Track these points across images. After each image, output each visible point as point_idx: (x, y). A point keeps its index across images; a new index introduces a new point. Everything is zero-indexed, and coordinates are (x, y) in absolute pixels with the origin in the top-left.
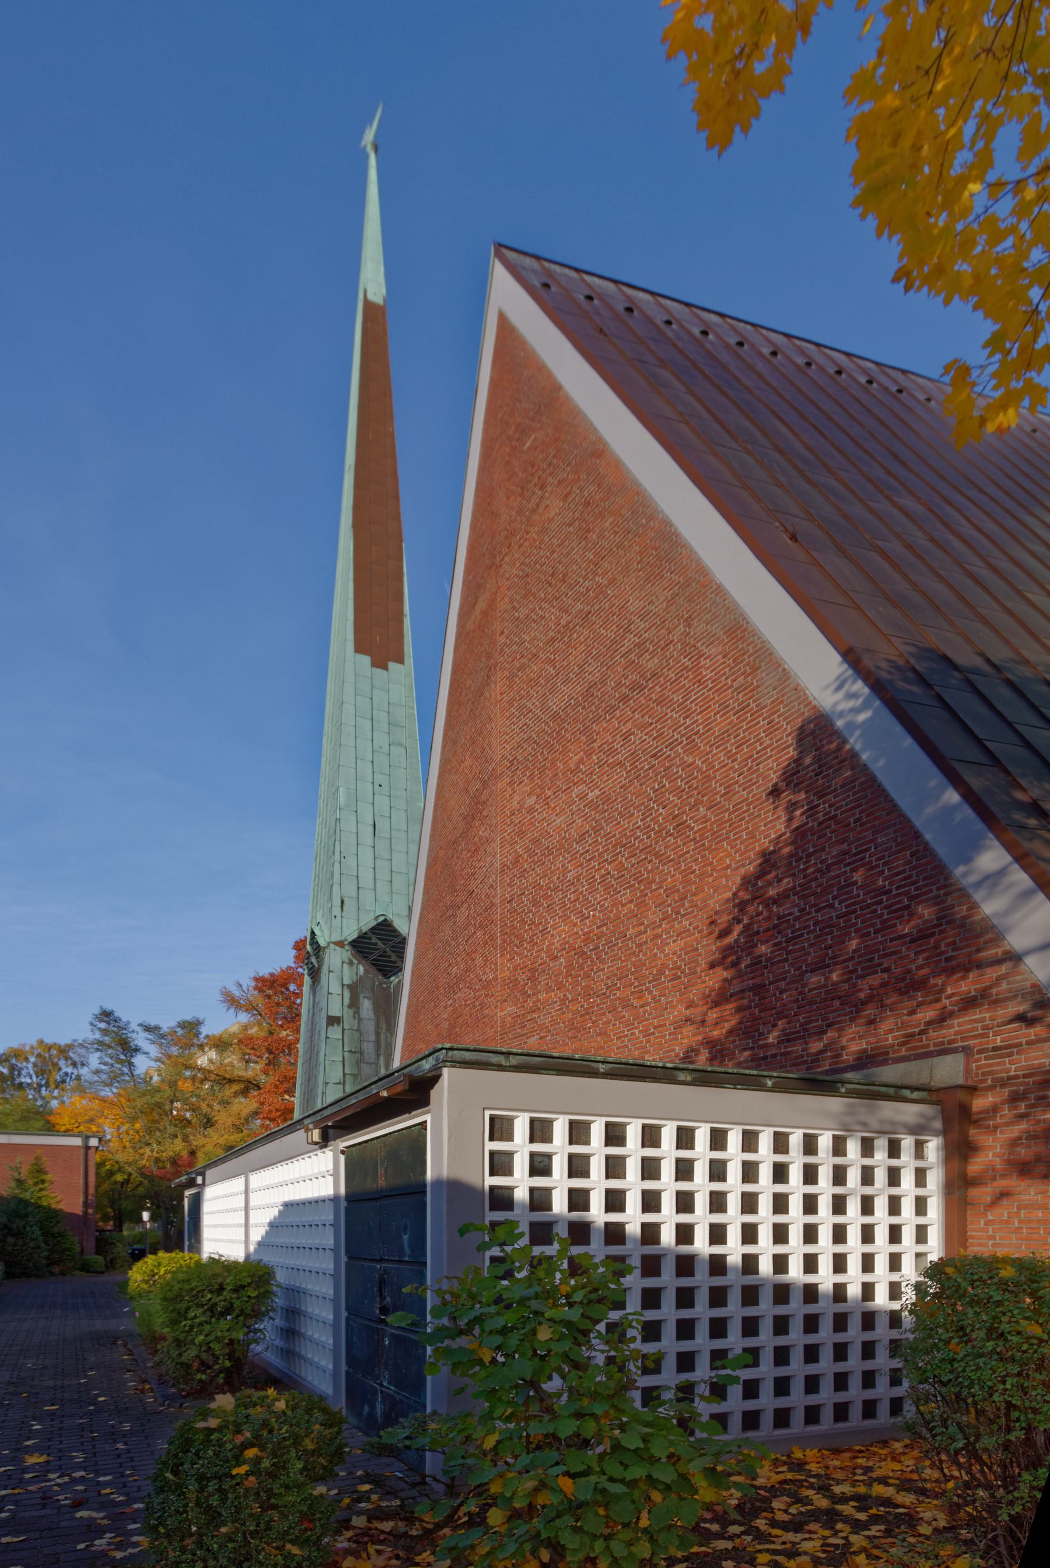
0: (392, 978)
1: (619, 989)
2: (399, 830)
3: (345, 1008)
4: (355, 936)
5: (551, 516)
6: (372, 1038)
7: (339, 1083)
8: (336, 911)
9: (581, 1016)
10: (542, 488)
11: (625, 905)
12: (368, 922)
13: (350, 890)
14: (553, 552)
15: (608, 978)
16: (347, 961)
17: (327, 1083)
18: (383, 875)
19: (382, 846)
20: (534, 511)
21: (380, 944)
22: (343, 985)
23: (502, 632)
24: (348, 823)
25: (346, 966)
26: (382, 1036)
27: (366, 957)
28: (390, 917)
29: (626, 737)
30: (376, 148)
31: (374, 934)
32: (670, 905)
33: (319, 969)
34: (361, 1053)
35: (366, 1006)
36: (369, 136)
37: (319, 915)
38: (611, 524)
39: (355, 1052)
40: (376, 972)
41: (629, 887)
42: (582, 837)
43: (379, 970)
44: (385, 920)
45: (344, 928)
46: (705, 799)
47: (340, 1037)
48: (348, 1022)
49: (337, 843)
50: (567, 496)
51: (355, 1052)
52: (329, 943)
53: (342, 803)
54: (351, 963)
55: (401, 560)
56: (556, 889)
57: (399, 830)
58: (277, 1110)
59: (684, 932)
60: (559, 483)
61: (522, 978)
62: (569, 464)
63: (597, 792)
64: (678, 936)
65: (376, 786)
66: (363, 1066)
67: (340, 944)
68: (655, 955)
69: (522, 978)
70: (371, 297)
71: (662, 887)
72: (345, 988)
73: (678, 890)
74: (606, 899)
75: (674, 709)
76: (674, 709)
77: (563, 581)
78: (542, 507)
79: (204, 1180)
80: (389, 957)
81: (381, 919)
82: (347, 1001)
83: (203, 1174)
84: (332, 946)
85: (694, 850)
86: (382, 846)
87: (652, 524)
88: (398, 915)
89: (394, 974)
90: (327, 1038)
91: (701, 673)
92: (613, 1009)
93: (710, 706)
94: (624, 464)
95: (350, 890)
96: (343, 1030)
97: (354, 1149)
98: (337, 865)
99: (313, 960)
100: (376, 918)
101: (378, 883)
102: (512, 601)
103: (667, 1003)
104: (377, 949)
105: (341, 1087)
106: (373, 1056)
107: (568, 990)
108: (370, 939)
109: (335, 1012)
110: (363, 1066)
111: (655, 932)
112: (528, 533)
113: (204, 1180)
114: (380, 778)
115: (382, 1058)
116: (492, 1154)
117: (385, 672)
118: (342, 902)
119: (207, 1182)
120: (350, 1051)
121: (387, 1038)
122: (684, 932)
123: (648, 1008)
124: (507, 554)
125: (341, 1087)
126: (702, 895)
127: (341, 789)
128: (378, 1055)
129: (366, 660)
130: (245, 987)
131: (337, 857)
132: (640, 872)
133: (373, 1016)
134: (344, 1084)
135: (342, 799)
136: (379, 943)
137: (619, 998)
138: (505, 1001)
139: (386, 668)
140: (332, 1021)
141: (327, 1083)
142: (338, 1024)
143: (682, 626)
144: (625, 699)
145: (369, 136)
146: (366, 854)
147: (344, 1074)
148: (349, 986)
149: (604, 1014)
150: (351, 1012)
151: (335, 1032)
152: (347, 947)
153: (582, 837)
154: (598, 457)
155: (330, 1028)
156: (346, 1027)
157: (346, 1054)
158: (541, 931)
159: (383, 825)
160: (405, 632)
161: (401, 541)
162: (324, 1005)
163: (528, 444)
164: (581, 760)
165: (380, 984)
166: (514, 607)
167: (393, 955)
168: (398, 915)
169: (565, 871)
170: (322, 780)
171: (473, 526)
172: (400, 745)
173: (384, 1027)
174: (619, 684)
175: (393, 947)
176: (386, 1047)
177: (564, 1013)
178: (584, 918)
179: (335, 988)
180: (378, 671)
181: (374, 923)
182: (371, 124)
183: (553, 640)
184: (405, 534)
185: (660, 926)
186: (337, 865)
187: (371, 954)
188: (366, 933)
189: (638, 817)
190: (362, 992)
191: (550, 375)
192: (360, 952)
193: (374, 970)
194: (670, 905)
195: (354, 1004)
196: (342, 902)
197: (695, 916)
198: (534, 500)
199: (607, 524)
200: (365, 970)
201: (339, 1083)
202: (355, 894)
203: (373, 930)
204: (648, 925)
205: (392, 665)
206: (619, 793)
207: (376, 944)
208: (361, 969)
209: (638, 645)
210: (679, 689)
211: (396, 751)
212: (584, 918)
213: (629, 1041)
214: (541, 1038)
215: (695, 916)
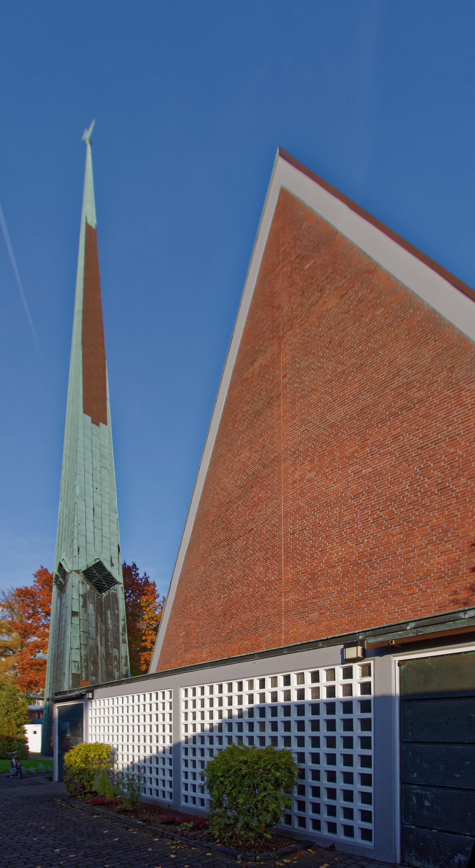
0: (103, 594)
1: (390, 584)
2: (105, 514)
3: (81, 607)
4: (85, 568)
5: (329, 307)
6: (94, 625)
7: (78, 649)
8: (76, 553)
9: (356, 601)
10: (320, 291)
11: (396, 535)
12: (91, 562)
13: (83, 544)
14: (331, 329)
15: (381, 578)
16: (81, 581)
17: (72, 648)
18: (98, 538)
19: (98, 521)
20: (313, 305)
21: (97, 575)
22: (79, 595)
23: (285, 376)
24: (81, 506)
25: (80, 584)
26: (99, 624)
27: (91, 581)
28: (102, 560)
29: (396, 437)
30: (91, 143)
31: (95, 568)
32: (435, 535)
33: (65, 585)
34: (89, 633)
35: (91, 607)
36: (87, 135)
37: (63, 556)
38: (382, 313)
39: (86, 632)
40: (96, 589)
41: (398, 525)
42: (356, 496)
43: (98, 589)
44: (100, 562)
45: (80, 563)
46: (465, 473)
47: (78, 623)
48: (82, 615)
49: (76, 516)
50: (343, 296)
51: (86, 632)
52: (71, 571)
53: (78, 494)
54: (83, 583)
55: (105, 369)
56: (333, 527)
57: (105, 514)
58: (28, 664)
59: (447, 551)
60: (336, 289)
61: (303, 578)
62: (344, 277)
63: (370, 470)
64: (442, 553)
65: (95, 488)
66: (90, 640)
67: (78, 572)
68: (423, 564)
69: (303, 578)
70: (89, 222)
71: (428, 525)
72: (80, 596)
73: (442, 527)
74: (379, 532)
75: (438, 421)
76: (438, 421)
77: (340, 345)
78: (321, 302)
79: (93, 695)
80: (102, 582)
81: (98, 561)
82: (81, 604)
83: (92, 692)
84: (74, 572)
85: (455, 503)
86: (98, 521)
87: (418, 313)
88: (105, 560)
89: (105, 591)
90: (72, 623)
91: (462, 400)
92: (385, 596)
93: (470, 419)
94: (394, 277)
95: (83, 544)
96: (80, 619)
97: (417, 661)
98: (76, 528)
99: (61, 579)
100: (95, 560)
101: (96, 540)
102: (293, 357)
103: (432, 593)
104: (96, 577)
105: (79, 651)
106: (94, 635)
107: (345, 585)
108: (92, 571)
109: (76, 609)
110: (90, 640)
111: (422, 551)
112: (308, 318)
113: (93, 695)
114: (96, 485)
115: (99, 636)
116: (370, 675)
117: (98, 427)
118: (79, 549)
119: (95, 697)
120: (83, 632)
121: (101, 625)
122: (447, 551)
123: (415, 595)
124: (289, 330)
125: (79, 651)
126: (462, 530)
127: (77, 486)
128: (97, 635)
129: (89, 419)
130: (7, 595)
131: (76, 523)
132: (409, 516)
133: (94, 613)
134: (80, 649)
135: (78, 493)
136: (97, 573)
137: (391, 590)
138: (289, 592)
139: (98, 425)
140: (74, 614)
141: (72, 648)
142: (77, 616)
143: (445, 372)
144: (395, 415)
145: (87, 135)
146: (90, 525)
147: (81, 644)
148: (82, 596)
149: (377, 599)
150: (83, 610)
151: (76, 620)
152: (81, 574)
153: (356, 496)
154: (371, 273)
155: (73, 617)
156: (81, 618)
157: (81, 633)
158: (321, 551)
159: (98, 510)
160: (107, 408)
161: (105, 359)
162: (69, 604)
163: (308, 266)
164: (356, 451)
165: (98, 596)
166: (296, 362)
167: (104, 581)
168: (105, 560)
169: (341, 516)
170: (62, 481)
171: (251, 316)
172: (106, 468)
173: (100, 620)
174: (389, 407)
175: (104, 577)
176: (101, 630)
177: (342, 599)
178: (358, 544)
179: (76, 596)
180: (95, 426)
181: (94, 563)
182: (88, 129)
183: (330, 381)
184: (107, 356)
185: (426, 547)
186: (76, 528)
187: (93, 579)
188: (90, 567)
189: (406, 484)
190: (89, 599)
191: (327, 225)
192: (88, 577)
193: (94, 588)
194: (435, 535)
195: (85, 606)
196: (79, 549)
197: (458, 542)
198: (313, 299)
199: (379, 312)
200: (90, 588)
201: (78, 649)
202: (85, 546)
203: (95, 566)
204: (416, 547)
205: (101, 424)
206: (389, 470)
207: (95, 574)
208: (88, 587)
209: (407, 384)
210: (442, 409)
211: (104, 471)
212: (358, 544)
213: (399, 614)
214: (321, 614)
215: (458, 542)
